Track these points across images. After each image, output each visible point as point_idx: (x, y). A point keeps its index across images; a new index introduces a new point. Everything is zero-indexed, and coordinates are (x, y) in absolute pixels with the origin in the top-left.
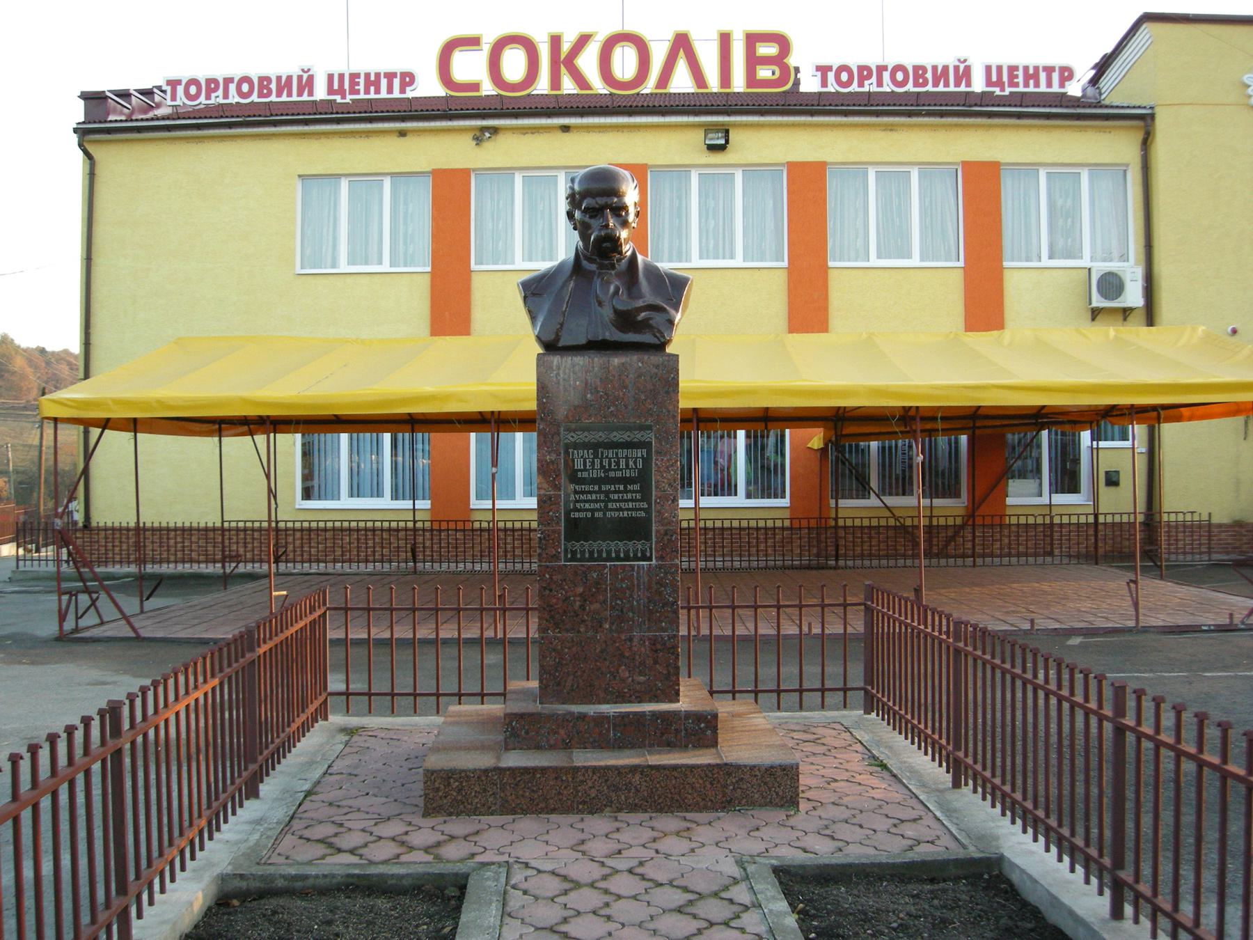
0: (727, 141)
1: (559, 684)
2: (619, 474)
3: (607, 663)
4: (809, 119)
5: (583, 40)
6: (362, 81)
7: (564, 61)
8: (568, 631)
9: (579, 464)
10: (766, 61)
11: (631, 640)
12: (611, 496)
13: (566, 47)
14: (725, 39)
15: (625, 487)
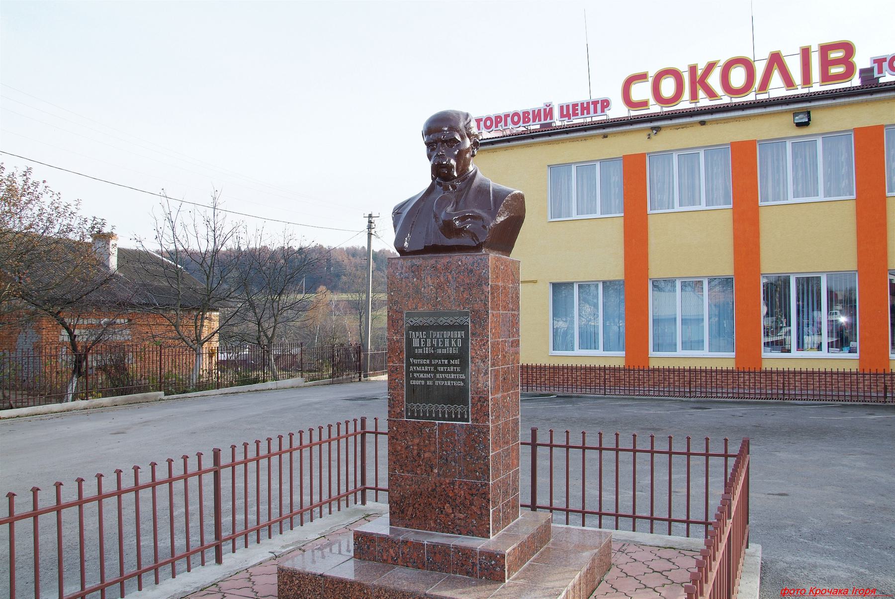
0: (809, 120)
1: (403, 512)
2: (444, 351)
3: (436, 500)
4: (869, 97)
5: (710, 67)
6: (579, 107)
7: (699, 81)
8: (408, 472)
9: (416, 343)
10: (836, 62)
11: (453, 483)
12: (439, 368)
13: (699, 72)
14: (806, 53)
15: (449, 362)
